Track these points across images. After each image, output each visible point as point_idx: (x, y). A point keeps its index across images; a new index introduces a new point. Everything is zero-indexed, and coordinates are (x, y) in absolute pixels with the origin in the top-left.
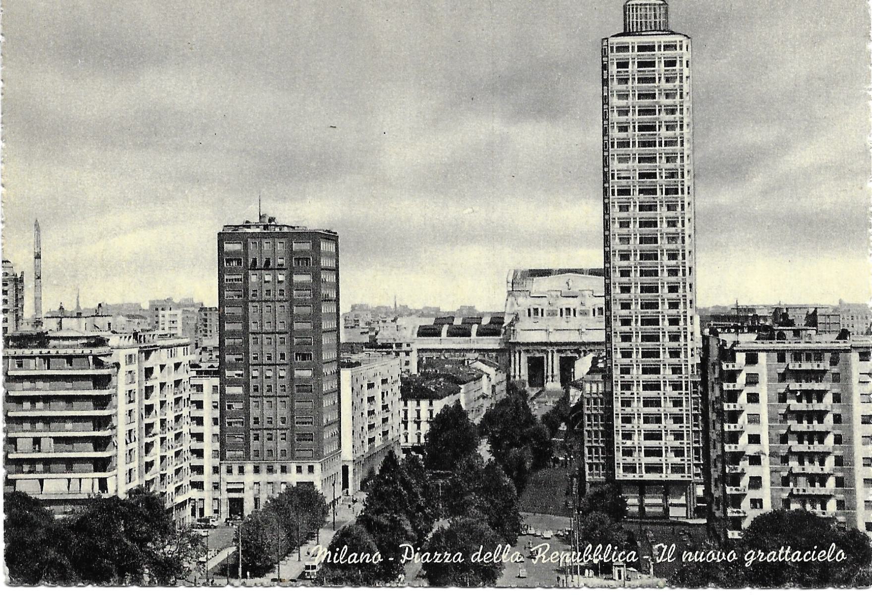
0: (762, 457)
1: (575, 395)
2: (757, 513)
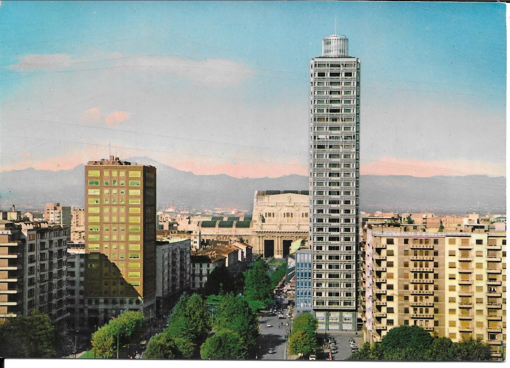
0: (394, 297)
1: (291, 263)
2: (390, 328)
